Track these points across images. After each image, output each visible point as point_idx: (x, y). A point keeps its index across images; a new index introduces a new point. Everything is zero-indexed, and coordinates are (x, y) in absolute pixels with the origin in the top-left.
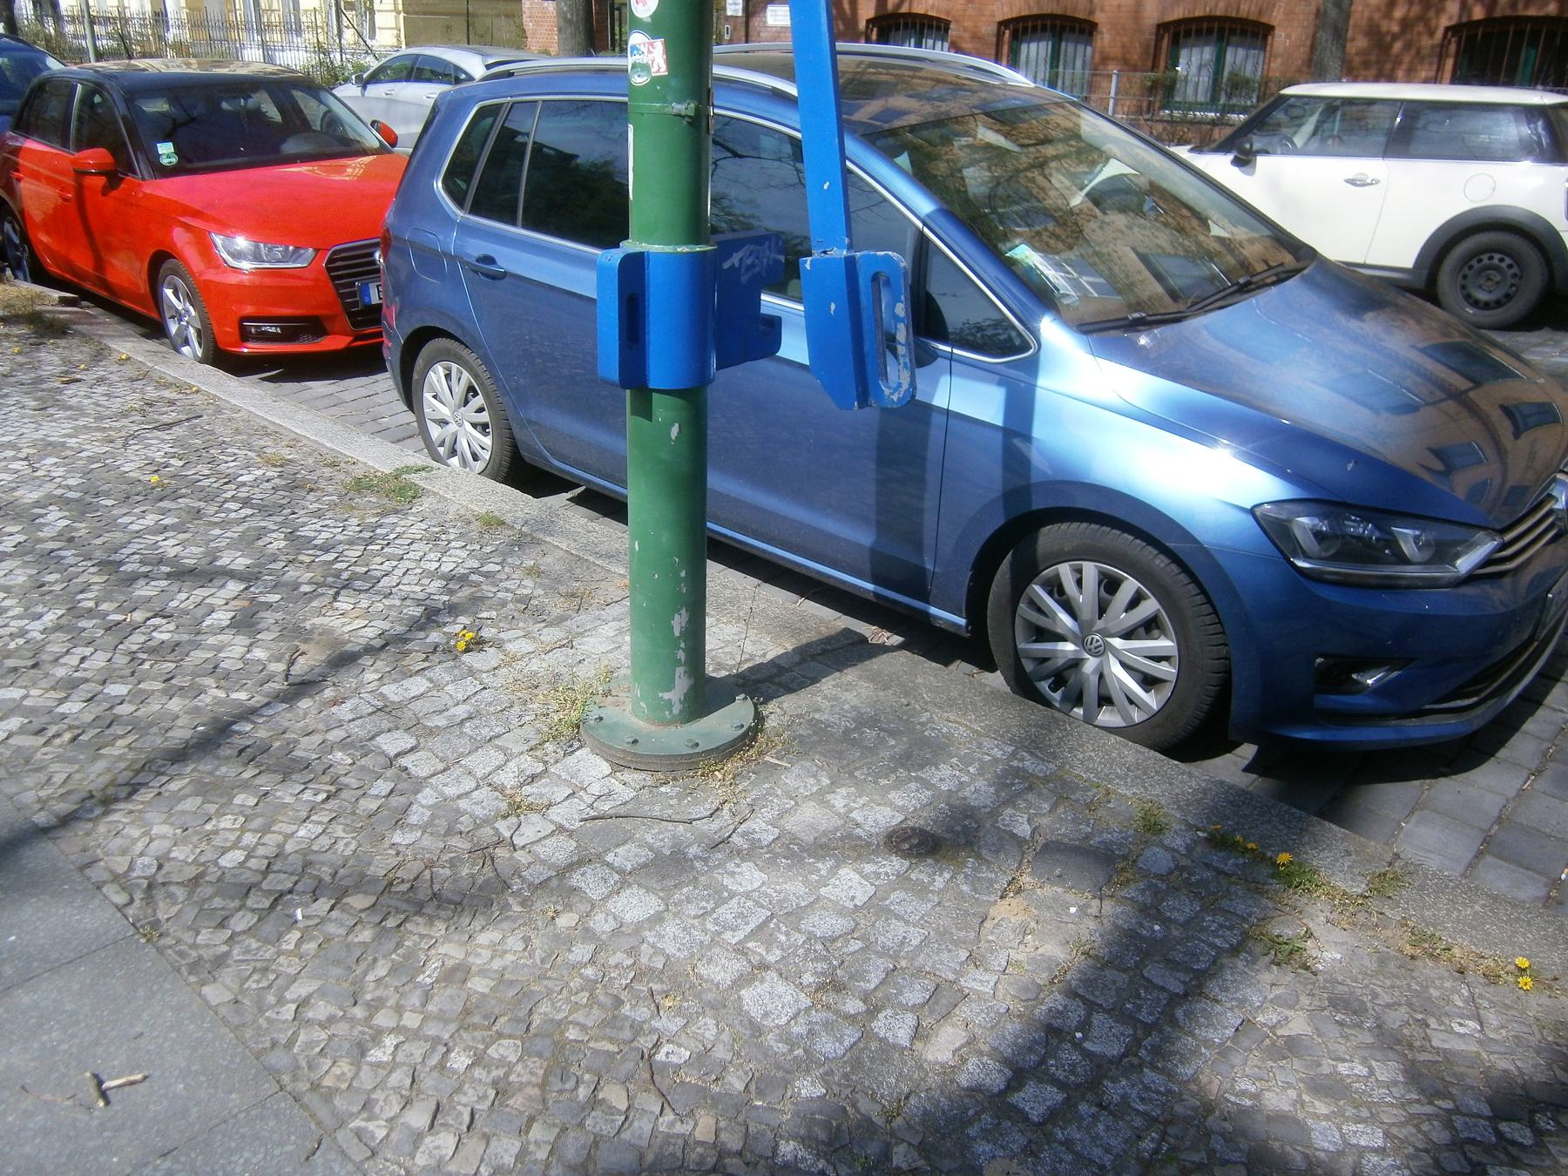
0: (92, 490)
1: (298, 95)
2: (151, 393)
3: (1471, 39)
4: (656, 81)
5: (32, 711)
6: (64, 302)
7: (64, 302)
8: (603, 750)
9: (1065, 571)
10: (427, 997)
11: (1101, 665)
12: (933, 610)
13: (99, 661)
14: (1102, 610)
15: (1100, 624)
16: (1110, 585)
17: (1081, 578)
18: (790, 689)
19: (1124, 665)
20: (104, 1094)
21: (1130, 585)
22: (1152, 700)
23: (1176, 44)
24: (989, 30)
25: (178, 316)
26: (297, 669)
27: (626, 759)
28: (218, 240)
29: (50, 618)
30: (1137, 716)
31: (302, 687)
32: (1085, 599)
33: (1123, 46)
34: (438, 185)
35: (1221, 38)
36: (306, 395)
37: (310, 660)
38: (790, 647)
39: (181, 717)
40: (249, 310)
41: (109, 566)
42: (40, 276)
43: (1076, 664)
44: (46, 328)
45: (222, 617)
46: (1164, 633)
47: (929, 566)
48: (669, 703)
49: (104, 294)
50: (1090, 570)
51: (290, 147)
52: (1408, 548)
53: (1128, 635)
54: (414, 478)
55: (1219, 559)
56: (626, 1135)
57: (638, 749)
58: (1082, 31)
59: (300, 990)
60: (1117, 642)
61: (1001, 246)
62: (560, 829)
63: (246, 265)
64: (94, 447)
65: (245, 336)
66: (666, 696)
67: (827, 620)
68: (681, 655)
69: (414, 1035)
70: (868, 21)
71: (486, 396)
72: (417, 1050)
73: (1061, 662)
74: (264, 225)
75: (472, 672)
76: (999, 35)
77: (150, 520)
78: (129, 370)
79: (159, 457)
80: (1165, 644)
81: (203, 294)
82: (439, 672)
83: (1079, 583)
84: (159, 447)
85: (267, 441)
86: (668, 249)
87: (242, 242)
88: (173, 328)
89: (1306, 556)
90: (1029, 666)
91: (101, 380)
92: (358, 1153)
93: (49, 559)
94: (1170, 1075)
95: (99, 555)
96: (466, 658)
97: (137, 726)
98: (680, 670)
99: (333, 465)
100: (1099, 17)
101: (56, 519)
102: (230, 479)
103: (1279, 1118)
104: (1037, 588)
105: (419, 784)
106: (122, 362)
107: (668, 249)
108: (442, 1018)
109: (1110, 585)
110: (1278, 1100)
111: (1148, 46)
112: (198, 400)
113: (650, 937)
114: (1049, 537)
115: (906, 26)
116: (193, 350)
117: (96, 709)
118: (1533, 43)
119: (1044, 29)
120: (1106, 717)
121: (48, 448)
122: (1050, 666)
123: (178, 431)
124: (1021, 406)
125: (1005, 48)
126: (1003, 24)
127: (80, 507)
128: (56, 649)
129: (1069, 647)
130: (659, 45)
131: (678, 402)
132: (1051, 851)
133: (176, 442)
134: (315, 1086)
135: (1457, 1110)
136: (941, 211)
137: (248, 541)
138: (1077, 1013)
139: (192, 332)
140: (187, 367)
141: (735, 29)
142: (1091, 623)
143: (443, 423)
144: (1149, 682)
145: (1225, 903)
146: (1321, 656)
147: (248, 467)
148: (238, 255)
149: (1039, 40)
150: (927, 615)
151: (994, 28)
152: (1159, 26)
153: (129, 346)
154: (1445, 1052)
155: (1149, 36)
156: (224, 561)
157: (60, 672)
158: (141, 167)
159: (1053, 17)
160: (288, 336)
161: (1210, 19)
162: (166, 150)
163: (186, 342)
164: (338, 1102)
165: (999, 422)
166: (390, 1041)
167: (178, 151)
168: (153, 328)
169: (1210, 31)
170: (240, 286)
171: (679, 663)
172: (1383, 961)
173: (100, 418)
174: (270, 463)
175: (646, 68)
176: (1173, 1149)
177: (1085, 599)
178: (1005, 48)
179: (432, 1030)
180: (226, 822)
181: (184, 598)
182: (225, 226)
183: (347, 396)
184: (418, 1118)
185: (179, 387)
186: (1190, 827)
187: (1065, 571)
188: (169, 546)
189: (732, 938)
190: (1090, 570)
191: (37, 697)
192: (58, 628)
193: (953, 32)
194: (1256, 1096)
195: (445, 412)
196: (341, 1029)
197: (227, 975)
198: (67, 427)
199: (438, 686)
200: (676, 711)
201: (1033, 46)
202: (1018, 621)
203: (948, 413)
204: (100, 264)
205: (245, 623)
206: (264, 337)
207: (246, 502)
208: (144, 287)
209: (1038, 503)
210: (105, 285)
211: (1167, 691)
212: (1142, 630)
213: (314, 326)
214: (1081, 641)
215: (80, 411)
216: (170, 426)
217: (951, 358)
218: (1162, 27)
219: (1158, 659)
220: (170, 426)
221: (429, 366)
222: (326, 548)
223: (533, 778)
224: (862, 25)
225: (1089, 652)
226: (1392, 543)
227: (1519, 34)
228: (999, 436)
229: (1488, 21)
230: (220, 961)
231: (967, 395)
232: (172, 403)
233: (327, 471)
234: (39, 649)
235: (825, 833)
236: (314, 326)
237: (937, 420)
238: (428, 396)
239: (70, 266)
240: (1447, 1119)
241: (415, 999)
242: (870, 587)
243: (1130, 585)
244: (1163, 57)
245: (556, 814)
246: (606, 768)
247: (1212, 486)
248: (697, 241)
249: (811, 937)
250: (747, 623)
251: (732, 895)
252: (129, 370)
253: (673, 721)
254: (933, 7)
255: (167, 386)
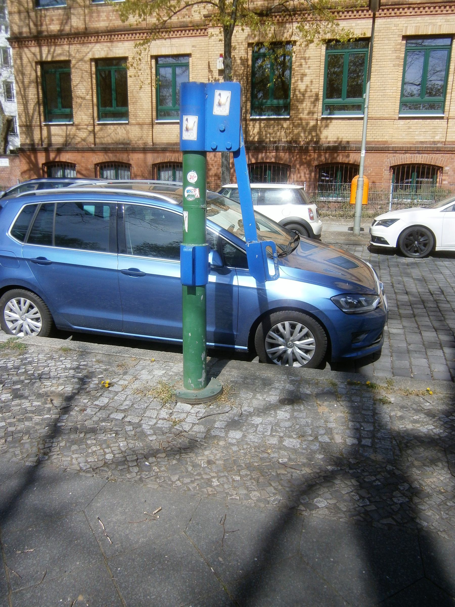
3: (252, 168)
4: (197, 199)
9: (279, 325)
11: (293, 351)
12: (236, 347)
14: (292, 334)
15: (291, 338)
16: (293, 327)
17: (284, 327)
19: (300, 349)
21: (299, 326)
22: (309, 357)
23: (159, 170)
24: (91, 167)
30: (305, 362)
32: (286, 332)
33: (141, 171)
34: (9, 234)
35: (174, 168)
43: (285, 352)
46: (311, 337)
47: (235, 333)
50: (287, 324)
53: (300, 340)
55: (325, 313)
56: (293, 477)
58: (126, 167)
60: (297, 343)
66: (200, 380)
70: (43, 164)
71: (39, 307)
73: (281, 352)
76: (96, 169)
80: (311, 340)
83: (284, 328)
86: (200, 245)
89: (345, 309)
90: (270, 356)
94: (386, 429)
98: (204, 371)
100: (131, 162)
103: (412, 430)
104: (271, 332)
107: (200, 245)
109: (293, 327)
110: (410, 426)
111: (150, 171)
114: (273, 317)
115: (58, 166)
118: (270, 169)
119: (112, 166)
122: (277, 354)
125: (98, 173)
126: (97, 165)
129: (282, 347)
130: (197, 190)
132: (318, 396)
135: (440, 418)
138: (358, 425)
142: (289, 339)
144: (307, 351)
145: (363, 395)
149: (110, 170)
150: (235, 348)
151: (94, 166)
152: (153, 165)
154: (428, 409)
155: (150, 168)
159: (115, 162)
161: (170, 162)
165: (255, 287)
169: (170, 166)
171: (203, 369)
172: (402, 397)
175: (193, 196)
176: (400, 442)
178: (98, 173)
186: (342, 382)
190: (287, 324)
193: (77, 167)
194: (405, 427)
195: (15, 316)
200: (203, 384)
201: (109, 172)
203: (238, 286)
209: (271, 307)
211: (313, 353)
214: (286, 345)
218: (154, 165)
219: (309, 345)
224: (40, 166)
225: (289, 347)
226: (359, 302)
227: (265, 167)
228: (256, 291)
229: (256, 163)
231: (244, 281)
235: (264, 405)
240: (440, 419)
242: (213, 344)
243: (299, 326)
244: (155, 175)
247: (317, 295)
251: (258, 425)
254: (68, 159)
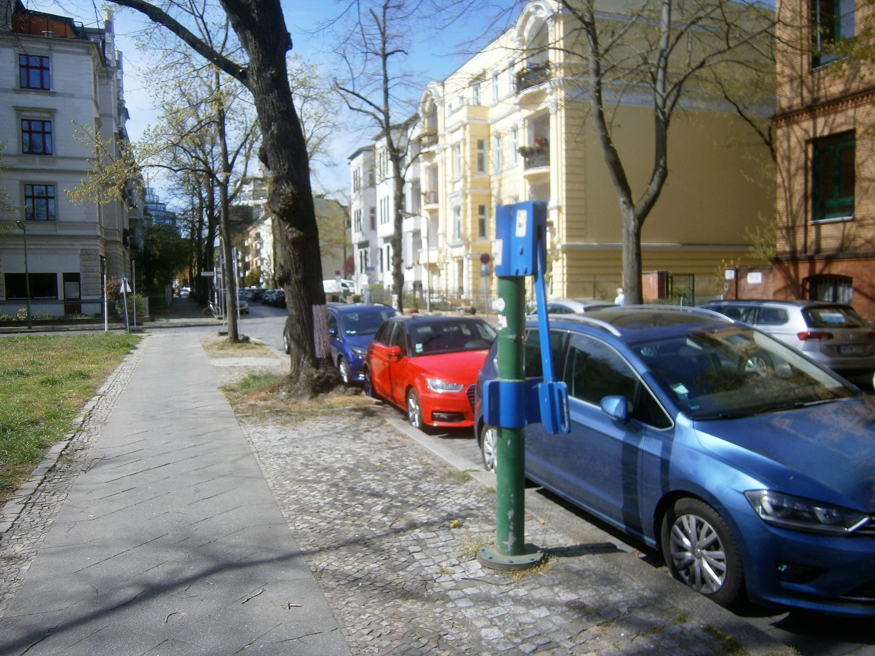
0: (357, 466)
1: (478, 325)
2: (393, 437)
4: (504, 329)
5: (312, 523)
6: (377, 404)
7: (377, 404)
8: (481, 561)
10: (385, 609)
13: (336, 513)
17: (689, 521)
18: (566, 556)
20: (290, 607)
21: (707, 525)
25: (413, 410)
26: (394, 526)
27: (487, 564)
28: (429, 380)
29: (328, 500)
31: (397, 532)
32: (691, 531)
36: (453, 444)
37: (400, 524)
38: (578, 544)
39: (352, 533)
40: (437, 408)
41: (351, 489)
42: (374, 395)
43: (691, 562)
44: (368, 413)
45: (379, 508)
48: (506, 547)
49: (392, 401)
50: (693, 518)
51: (468, 345)
52: (821, 517)
54: (471, 474)
57: (491, 560)
59: (350, 599)
61: (671, 386)
62: (454, 580)
63: (440, 391)
64: (364, 452)
65: (434, 418)
66: (506, 543)
67: (600, 536)
68: (511, 527)
69: (374, 615)
72: (374, 618)
74: (450, 375)
75: (453, 534)
77: (371, 477)
78: (389, 429)
79: (384, 458)
81: (424, 402)
82: (441, 533)
84: (386, 455)
85: (425, 457)
86: (507, 380)
87: (438, 382)
88: (411, 415)
90: (676, 563)
91: (377, 432)
92: (345, 633)
93: (335, 485)
95: (350, 485)
96: (453, 530)
97: (338, 532)
98: (511, 533)
99: (444, 467)
101: (342, 473)
102: (405, 467)
105: (415, 561)
106: (388, 426)
107: (507, 380)
108: (386, 614)
109: (700, 525)
112: (407, 441)
113: (463, 611)
114: (680, 504)
116: (417, 423)
117: (329, 526)
120: (704, 589)
121: (350, 451)
122: (683, 562)
123: (396, 450)
124: (667, 449)
127: (352, 471)
128: (325, 508)
131: (510, 432)
133: (393, 454)
134: (342, 619)
136: (648, 373)
137: (398, 488)
139: (416, 416)
140: (413, 432)
141: (731, 286)
143: (490, 454)
146: (785, 563)
147: (412, 464)
148: (435, 387)
150: (643, 540)
153: (393, 421)
156: (389, 492)
157: (324, 514)
158: (410, 354)
160: (450, 419)
162: (419, 347)
163: (414, 421)
164: (347, 624)
166: (367, 615)
167: (423, 348)
168: (404, 413)
170: (435, 399)
171: (510, 530)
173: (371, 444)
174: (421, 463)
177: (691, 531)
179: (381, 615)
180: (351, 559)
181: (369, 501)
182: (433, 375)
183: (468, 446)
184: (366, 631)
185: (403, 436)
187: (684, 518)
188: (373, 485)
189: (490, 616)
191: (315, 520)
192: (329, 503)
193: (855, 282)
196: (356, 610)
197: (333, 593)
198: (359, 445)
199: (438, 536)
202: (671, 542)
203: (643, 451)
204: (392, 390)
205: (385, 512)
206: (440, 419)
207: (406, 475)
208: (403, 400)
210: (393, 398)
212: (713, 547)
213: (460, 416)
215: (366, 441)
216: (393, 448)
217: (650, 430)
220: (393, 448)
221: (486, 431)
222: (424, 492)
223: (454, 565)
226: (813, 513)
230: (333, 589)
232: (398, 441)
233: (441, 469)
234: (321, 507)
236: (460, 416)
237: (640, 453)
238: (486, 443)
239: (383, 391)
241: (381, 608)
245: (454, 576)
246: (480, 566)
248: (517, 378)
249: (517, 621)
250: (548, 524)
252: (389, 429)
253: (508, 554)
255: (399, 435)
